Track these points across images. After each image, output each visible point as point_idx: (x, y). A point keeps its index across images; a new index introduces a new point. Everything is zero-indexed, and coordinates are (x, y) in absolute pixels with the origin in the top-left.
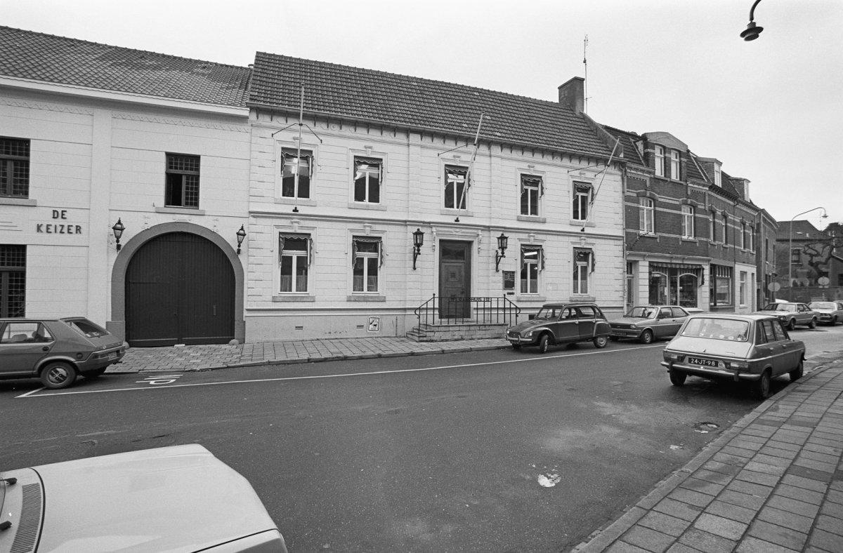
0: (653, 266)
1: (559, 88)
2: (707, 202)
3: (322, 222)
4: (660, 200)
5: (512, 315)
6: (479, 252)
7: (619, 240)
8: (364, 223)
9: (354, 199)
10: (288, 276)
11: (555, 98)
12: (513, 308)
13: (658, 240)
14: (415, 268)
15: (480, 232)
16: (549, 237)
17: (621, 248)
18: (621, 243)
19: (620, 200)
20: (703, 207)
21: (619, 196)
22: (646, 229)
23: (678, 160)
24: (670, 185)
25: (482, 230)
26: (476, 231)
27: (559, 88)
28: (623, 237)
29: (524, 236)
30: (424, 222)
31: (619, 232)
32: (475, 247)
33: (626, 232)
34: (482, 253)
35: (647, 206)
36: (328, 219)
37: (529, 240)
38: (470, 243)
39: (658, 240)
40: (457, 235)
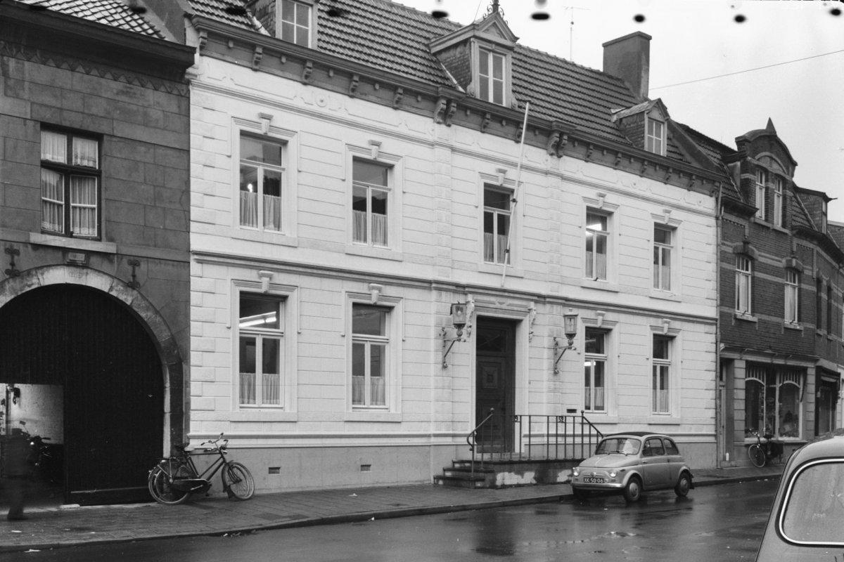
0: (751, 367)
1: (606, 45)
2: (815, 264)
3: (627, 316)
4: (761, 260)
5: (585, 446)
6: (530, 340)
7: (711, 324)
8: (370, 282)
9: (585, 275)
10: (252, 374)
11: (596, 62)
12: (594, 436)
13: (757, 326)
14: (445, 367)
15: (532, 305)
16: (622, 318)
17: (712, 338)
18: (713, 329)
19: (713, 258)
20: (810, 273)
21: (710, 252)
22: (743, 310)
23: (763, 185)
24: (772, 236)
25: (536, 302)
26: (524, 303)
27: (606, 45)
28: (716, 320)
29: (251, 275)
30: (457, 285)
31: (711, 311)
32: (523, 334)
33: (721, 312)
34: (536, 341)
35: (743, 269)
36: (634, 311)
37: (662, 328)
38: (514, 324)
39: (757, 326)
40: (500, 309)
